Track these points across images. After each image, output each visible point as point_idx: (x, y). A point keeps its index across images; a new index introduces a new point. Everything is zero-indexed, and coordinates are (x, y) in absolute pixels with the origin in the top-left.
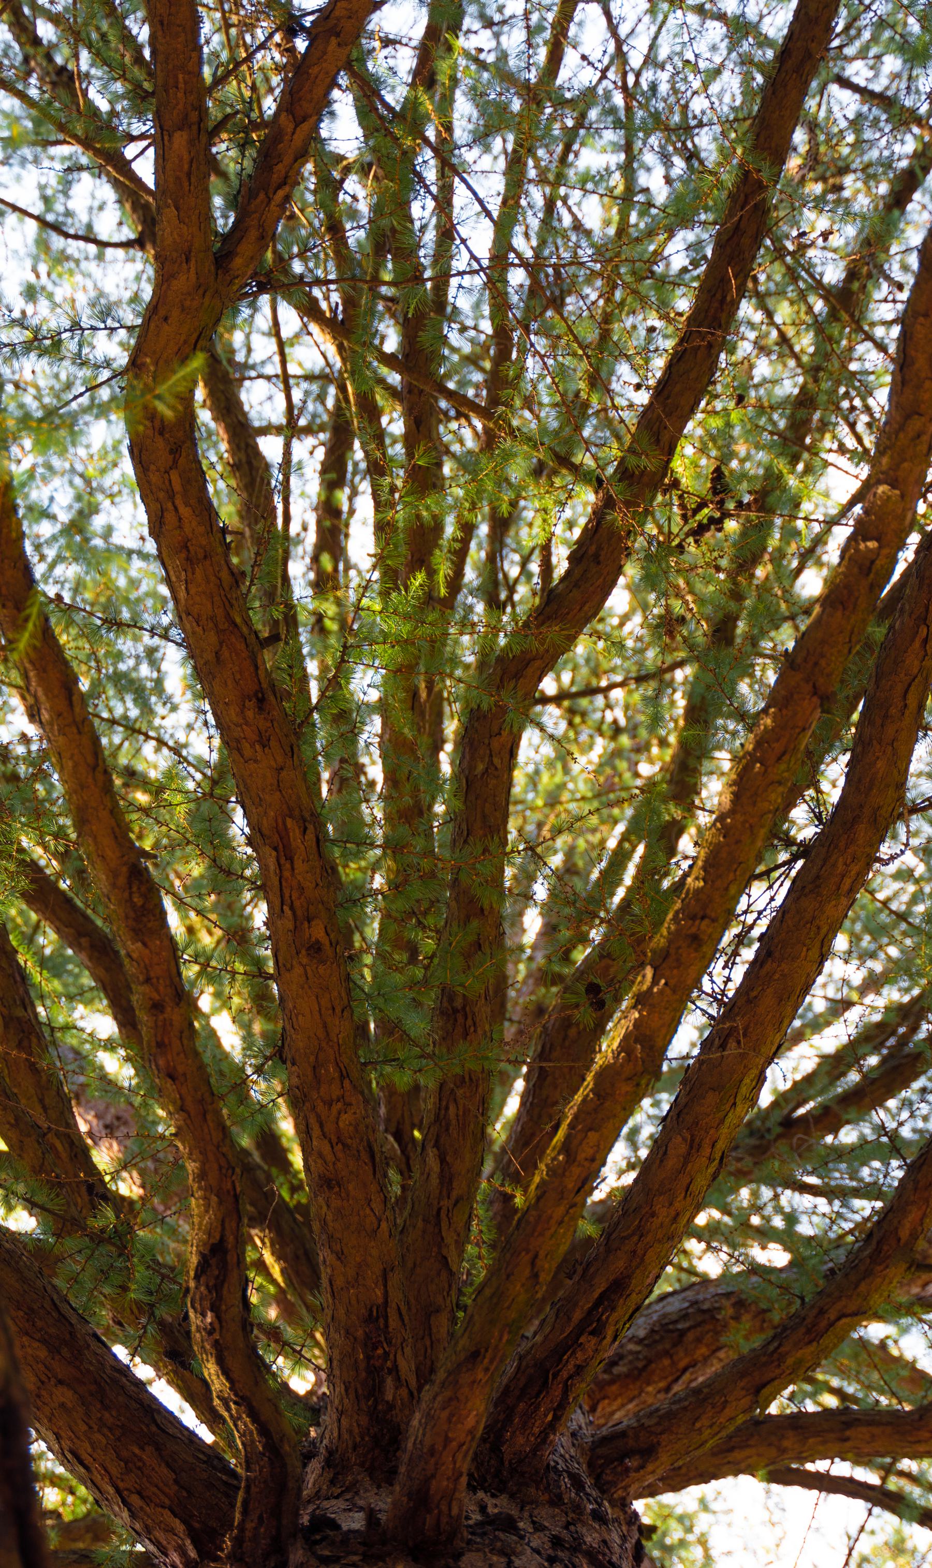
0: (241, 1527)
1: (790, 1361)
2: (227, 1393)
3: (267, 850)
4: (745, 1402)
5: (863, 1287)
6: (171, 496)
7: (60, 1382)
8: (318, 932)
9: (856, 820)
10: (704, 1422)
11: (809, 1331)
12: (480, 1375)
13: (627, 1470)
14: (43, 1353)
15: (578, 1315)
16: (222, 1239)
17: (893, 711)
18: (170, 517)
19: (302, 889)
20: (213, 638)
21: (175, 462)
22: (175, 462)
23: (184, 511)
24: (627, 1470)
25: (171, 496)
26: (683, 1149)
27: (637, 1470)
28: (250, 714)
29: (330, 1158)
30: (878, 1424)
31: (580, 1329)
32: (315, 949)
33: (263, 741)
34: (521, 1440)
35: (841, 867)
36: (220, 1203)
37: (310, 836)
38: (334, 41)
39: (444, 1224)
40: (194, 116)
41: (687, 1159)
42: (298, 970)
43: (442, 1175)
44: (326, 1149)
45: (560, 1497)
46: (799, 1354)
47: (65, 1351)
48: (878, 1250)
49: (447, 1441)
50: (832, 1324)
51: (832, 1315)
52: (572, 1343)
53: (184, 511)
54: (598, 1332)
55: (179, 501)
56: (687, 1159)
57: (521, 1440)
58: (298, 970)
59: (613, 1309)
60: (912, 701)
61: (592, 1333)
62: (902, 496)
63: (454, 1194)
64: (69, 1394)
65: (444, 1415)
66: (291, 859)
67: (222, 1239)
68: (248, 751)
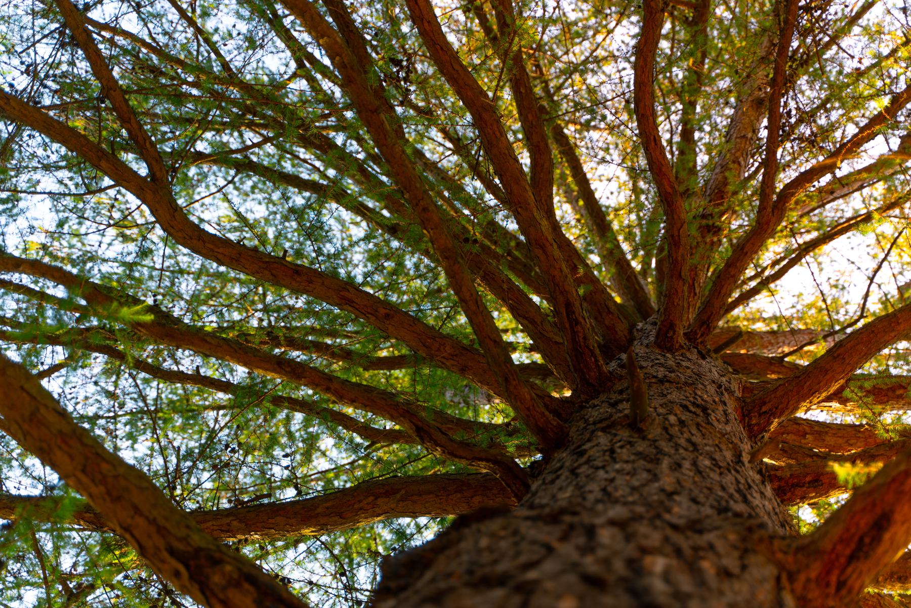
0: (513, 491)
1: (679, 258)
2: (468, 462)
3: (345, 307)
4: (681, 283)
5: (675, 217)
6: (212, 250)
7: (472, 497)
8: (382, 311)
9: (480, 116)
10: (676, 301)
11: (675, 245)
12: (514, 383)
13: (672, 337)
14: (459, 495)
15: (567, 326)
16: (417, 426)
17: (456, 76)
18: (219, 256)
19: (365, 306)
20: (266, 272)
21: (204, 241)
22: (204, 241)
23: (221, 250)
24: (672, 337)
25: (212, 250)
26: (541, 251)
27: (674, 333)
28: (298, 279)
29: (455, 363)
30: (750, 239)
31: (572, 327)
32: (387, 316)
33: (310, 282)
34: (593, 374)
35: (491, 132)
36: (404, 417)
37: (351, 290)
38: (112, 92)
39: (545, 334)
40: (100, 154)
41: (545, 252)
42: (390, 327)
43: (530, 323)
44: (453, 362)
45: (621, 376)
46: (680, 254)
47: (465, 488)
48: (668, 203)
49: (528, 409)
50: (679, 236)
51: (676, 233)
52: (574, 334)
53: (221, 250)
54: (577, 322)
55: (216, 250)
56: (545, 252)
57: (593, 374)
58: (390, 327)
59: (574, 313)
60: (457, 67)
61: (576, 325)
62: (329, 37)
63: (539, 323)
64: (478, 497)
65: (519, 403)
66: (353, 302)
67: (417, 426)
68: (310, 289)
